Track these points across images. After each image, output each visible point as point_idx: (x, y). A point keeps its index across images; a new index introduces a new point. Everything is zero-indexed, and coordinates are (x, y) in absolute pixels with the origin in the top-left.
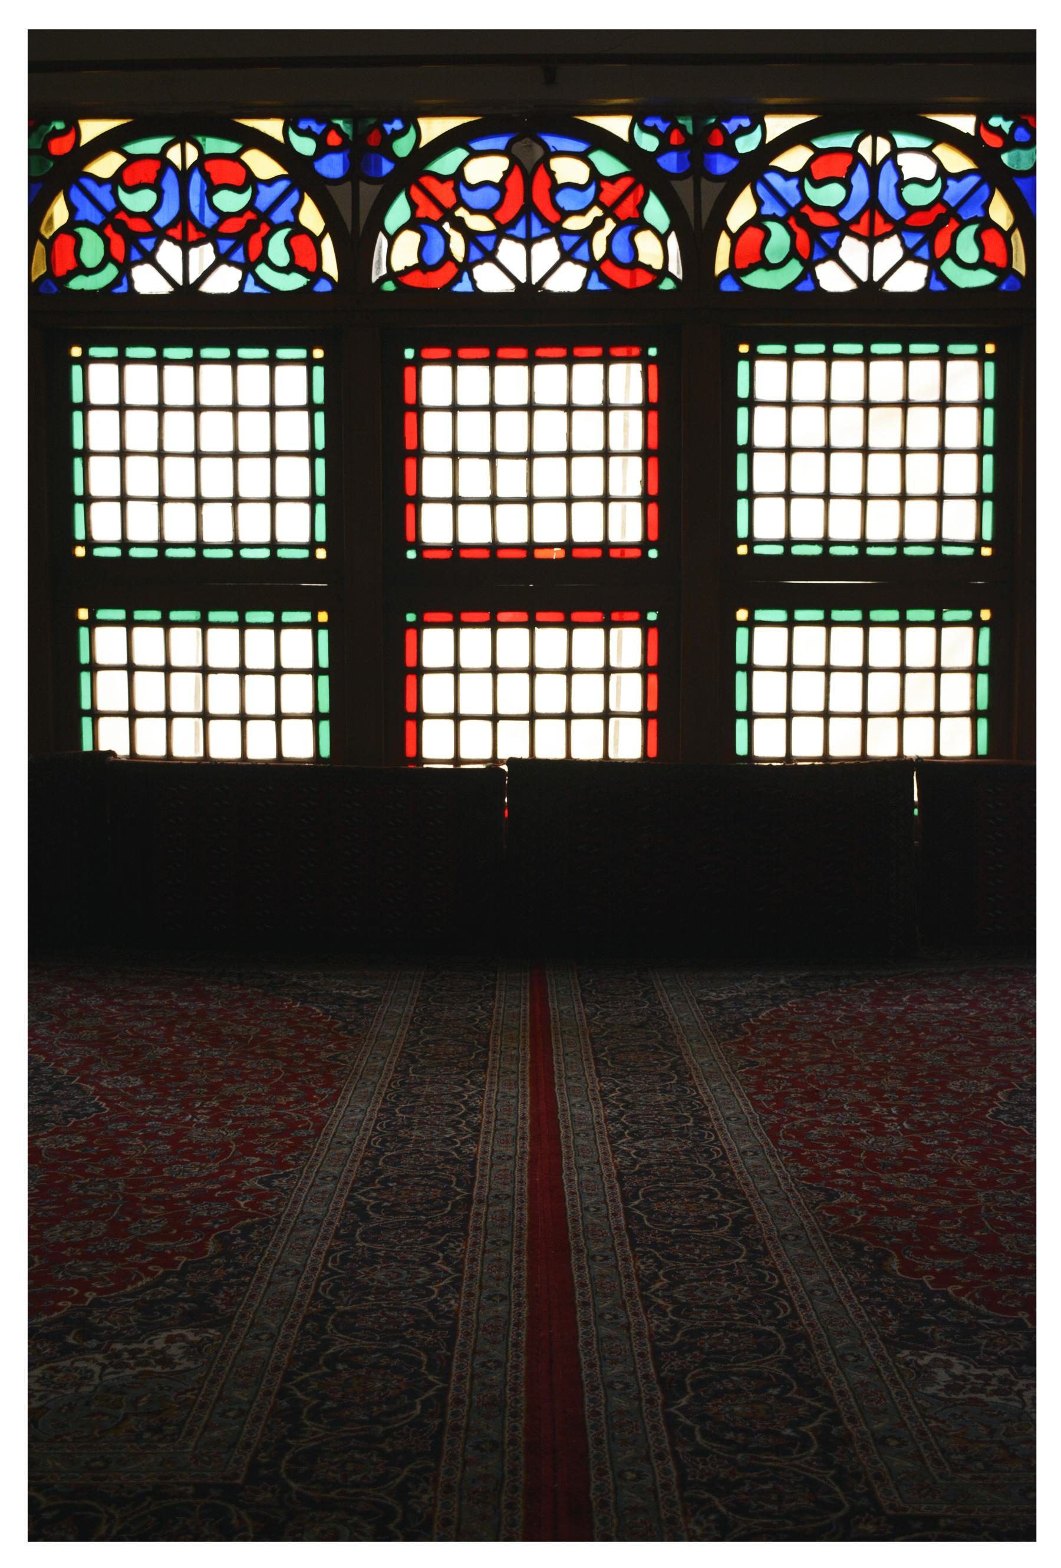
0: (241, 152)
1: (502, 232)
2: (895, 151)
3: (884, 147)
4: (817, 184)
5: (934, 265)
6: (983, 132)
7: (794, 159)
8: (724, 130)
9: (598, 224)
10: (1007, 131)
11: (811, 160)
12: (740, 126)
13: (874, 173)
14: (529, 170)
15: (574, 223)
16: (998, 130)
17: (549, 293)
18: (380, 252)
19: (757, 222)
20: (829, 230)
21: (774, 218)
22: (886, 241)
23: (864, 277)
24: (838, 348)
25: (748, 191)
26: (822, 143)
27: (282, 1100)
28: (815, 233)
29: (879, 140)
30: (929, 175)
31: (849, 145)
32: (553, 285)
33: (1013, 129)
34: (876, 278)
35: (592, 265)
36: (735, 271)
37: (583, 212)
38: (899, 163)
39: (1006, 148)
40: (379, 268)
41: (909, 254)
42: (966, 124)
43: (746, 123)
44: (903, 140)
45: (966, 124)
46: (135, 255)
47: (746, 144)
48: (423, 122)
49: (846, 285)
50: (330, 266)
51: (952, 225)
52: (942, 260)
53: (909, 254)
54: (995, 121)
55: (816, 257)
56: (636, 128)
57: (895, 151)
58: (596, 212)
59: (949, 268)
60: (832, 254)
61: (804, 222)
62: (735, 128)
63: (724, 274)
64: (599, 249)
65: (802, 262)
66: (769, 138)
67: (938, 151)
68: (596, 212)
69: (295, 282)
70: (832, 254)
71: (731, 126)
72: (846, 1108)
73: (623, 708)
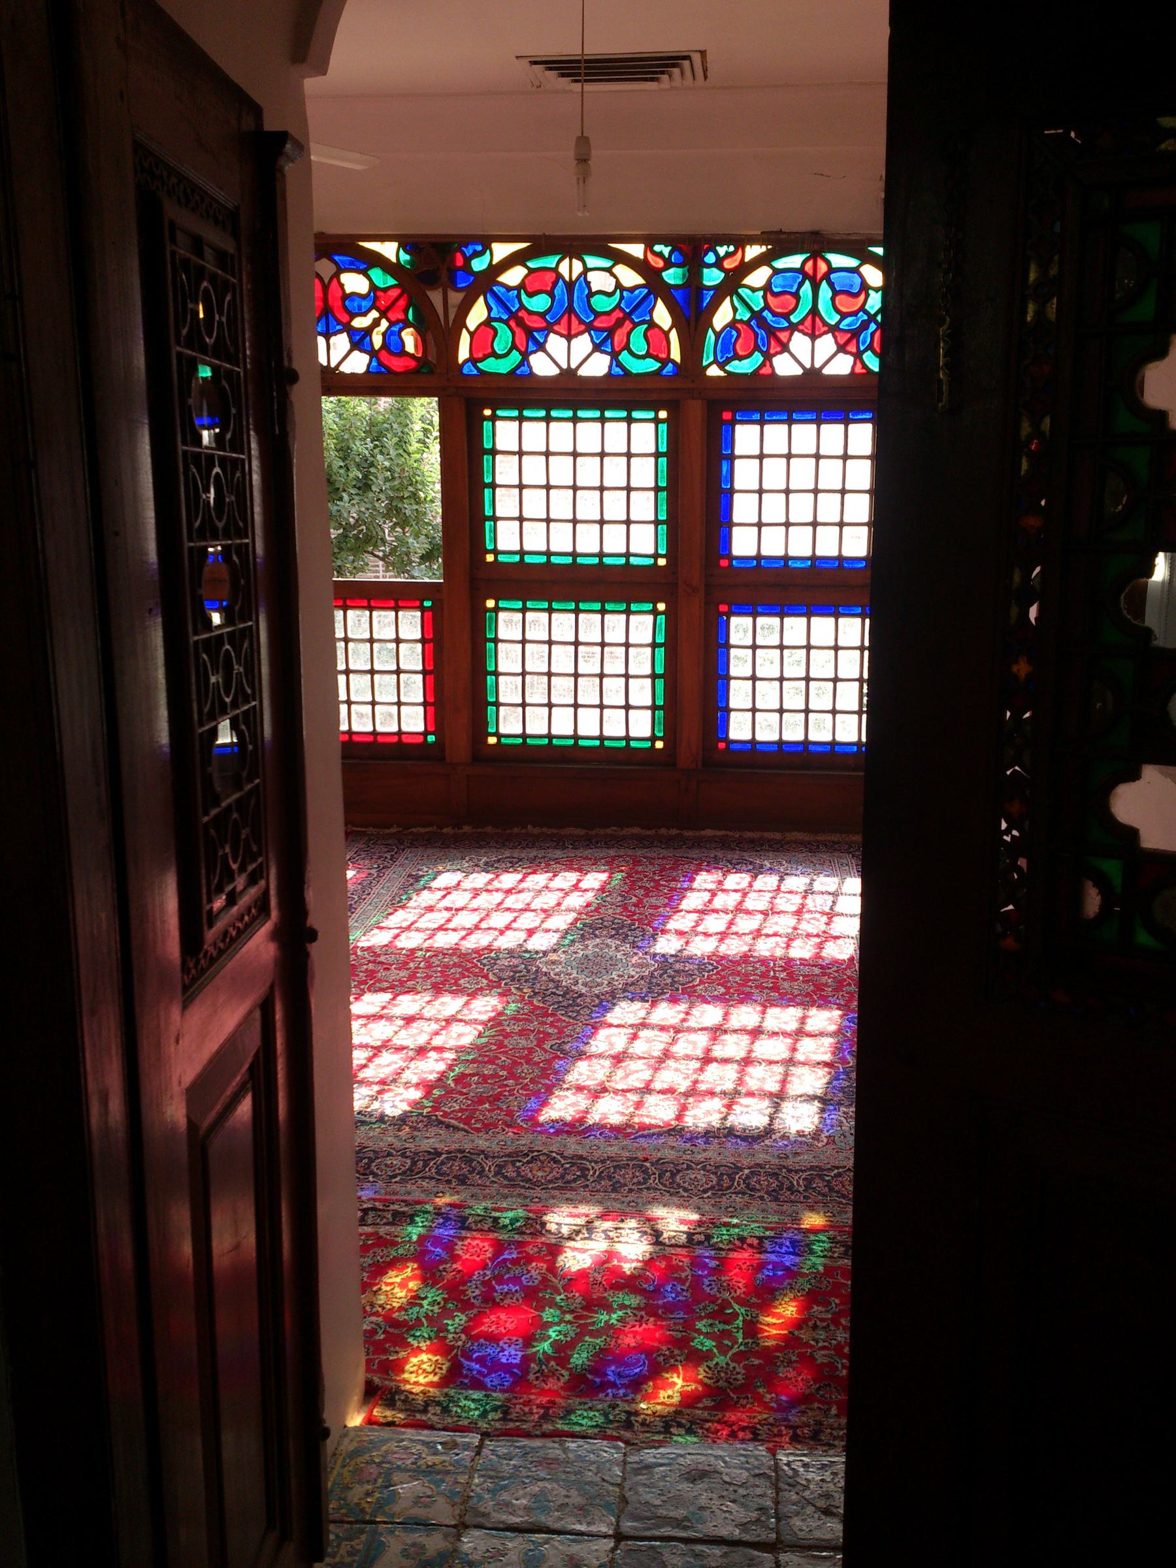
0: (860, 265)
1: (834, 329)
2: (586, 270)
3: (578, 267)
4: (530, 295)
5: (614, 355)
6: (650, 256)
7: (513, 276)
8: (463, 254)
9: (376, 323)
10: (667, 255)
11: (526, 276)
12: (475, 250)
13: (570, 286)
14: (326, 281)
15: (360, 323)
16: (660, 255)
17: (342, 373)
18: (708, 349)
19: (487, 323)
20: (783, 329)
21: (500, 320)
22: (580, 337)
23: (565, 366)
24: (554, 413)
25: (481, 299)
26: (532, 264)
27: (371, 966)
28: (529, 333)
29: (574, 261)
30: (610, 289)
31: (553, 266)
32: (346, 368)
33: (671, 253)
34: (573, 366)
35: (373, 353)
36: (473, 360)
37: (365, 314)
38: (589, 279)
39: (666, 268)
40: (708, 357)
41: (597, 348)
42: (636, 250)
43: (479, 248)
44: (592, 261)
45: (636, 250)
46: (532, 347)
47: (479, 265)
48: (495, 246)
49: (553, 371)
50: (676, 354)
51: (628, 325)
52: (620, 352)
53: (597, 348)
54: (658, 248)
55: (772, 351)
56: (401, 251)
57: (586, 270)
58: (374, 314)
59: (624, 357)
60: (541, 347)
61: (521, 323)
62: (471, 251)
63: (466, 362)
64: (377, 340)
65: (763, 353)
66: (747, 260)
67: (616, 270)
68: (374, 314)
69: (652, 365)
70: (541, 347)
71: (469, 251)
72: (801, 978)
73: (387, 677)
